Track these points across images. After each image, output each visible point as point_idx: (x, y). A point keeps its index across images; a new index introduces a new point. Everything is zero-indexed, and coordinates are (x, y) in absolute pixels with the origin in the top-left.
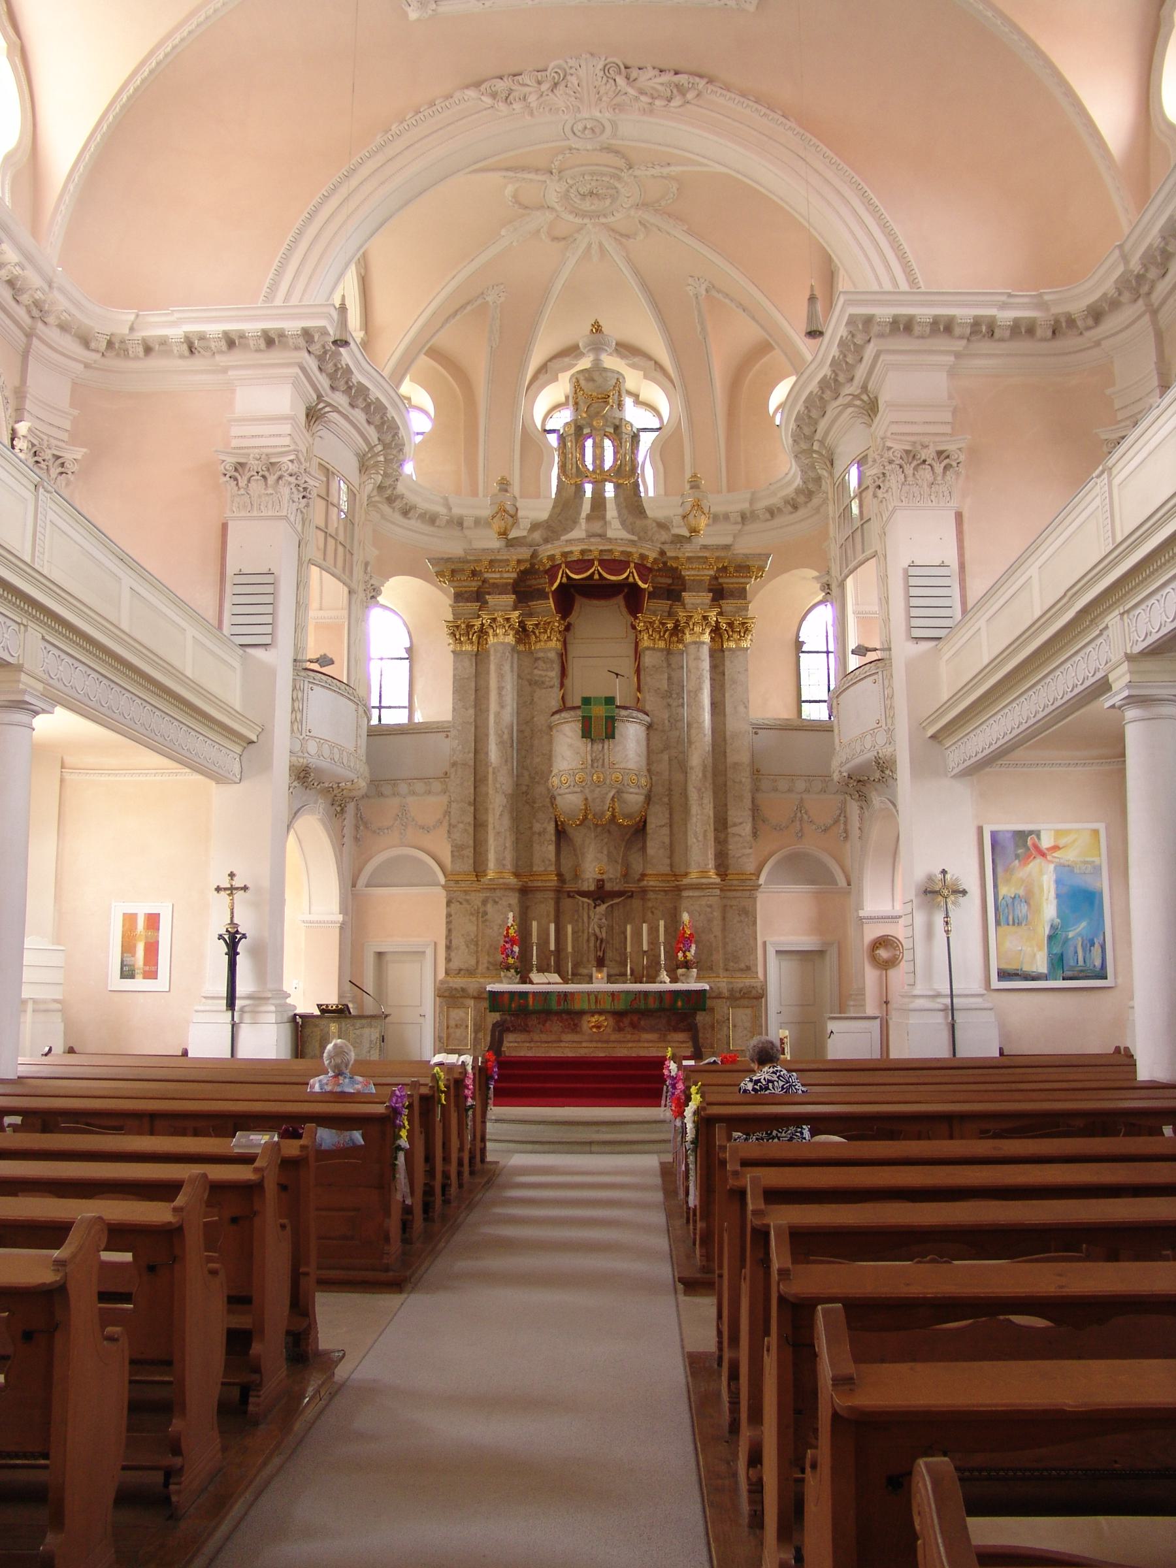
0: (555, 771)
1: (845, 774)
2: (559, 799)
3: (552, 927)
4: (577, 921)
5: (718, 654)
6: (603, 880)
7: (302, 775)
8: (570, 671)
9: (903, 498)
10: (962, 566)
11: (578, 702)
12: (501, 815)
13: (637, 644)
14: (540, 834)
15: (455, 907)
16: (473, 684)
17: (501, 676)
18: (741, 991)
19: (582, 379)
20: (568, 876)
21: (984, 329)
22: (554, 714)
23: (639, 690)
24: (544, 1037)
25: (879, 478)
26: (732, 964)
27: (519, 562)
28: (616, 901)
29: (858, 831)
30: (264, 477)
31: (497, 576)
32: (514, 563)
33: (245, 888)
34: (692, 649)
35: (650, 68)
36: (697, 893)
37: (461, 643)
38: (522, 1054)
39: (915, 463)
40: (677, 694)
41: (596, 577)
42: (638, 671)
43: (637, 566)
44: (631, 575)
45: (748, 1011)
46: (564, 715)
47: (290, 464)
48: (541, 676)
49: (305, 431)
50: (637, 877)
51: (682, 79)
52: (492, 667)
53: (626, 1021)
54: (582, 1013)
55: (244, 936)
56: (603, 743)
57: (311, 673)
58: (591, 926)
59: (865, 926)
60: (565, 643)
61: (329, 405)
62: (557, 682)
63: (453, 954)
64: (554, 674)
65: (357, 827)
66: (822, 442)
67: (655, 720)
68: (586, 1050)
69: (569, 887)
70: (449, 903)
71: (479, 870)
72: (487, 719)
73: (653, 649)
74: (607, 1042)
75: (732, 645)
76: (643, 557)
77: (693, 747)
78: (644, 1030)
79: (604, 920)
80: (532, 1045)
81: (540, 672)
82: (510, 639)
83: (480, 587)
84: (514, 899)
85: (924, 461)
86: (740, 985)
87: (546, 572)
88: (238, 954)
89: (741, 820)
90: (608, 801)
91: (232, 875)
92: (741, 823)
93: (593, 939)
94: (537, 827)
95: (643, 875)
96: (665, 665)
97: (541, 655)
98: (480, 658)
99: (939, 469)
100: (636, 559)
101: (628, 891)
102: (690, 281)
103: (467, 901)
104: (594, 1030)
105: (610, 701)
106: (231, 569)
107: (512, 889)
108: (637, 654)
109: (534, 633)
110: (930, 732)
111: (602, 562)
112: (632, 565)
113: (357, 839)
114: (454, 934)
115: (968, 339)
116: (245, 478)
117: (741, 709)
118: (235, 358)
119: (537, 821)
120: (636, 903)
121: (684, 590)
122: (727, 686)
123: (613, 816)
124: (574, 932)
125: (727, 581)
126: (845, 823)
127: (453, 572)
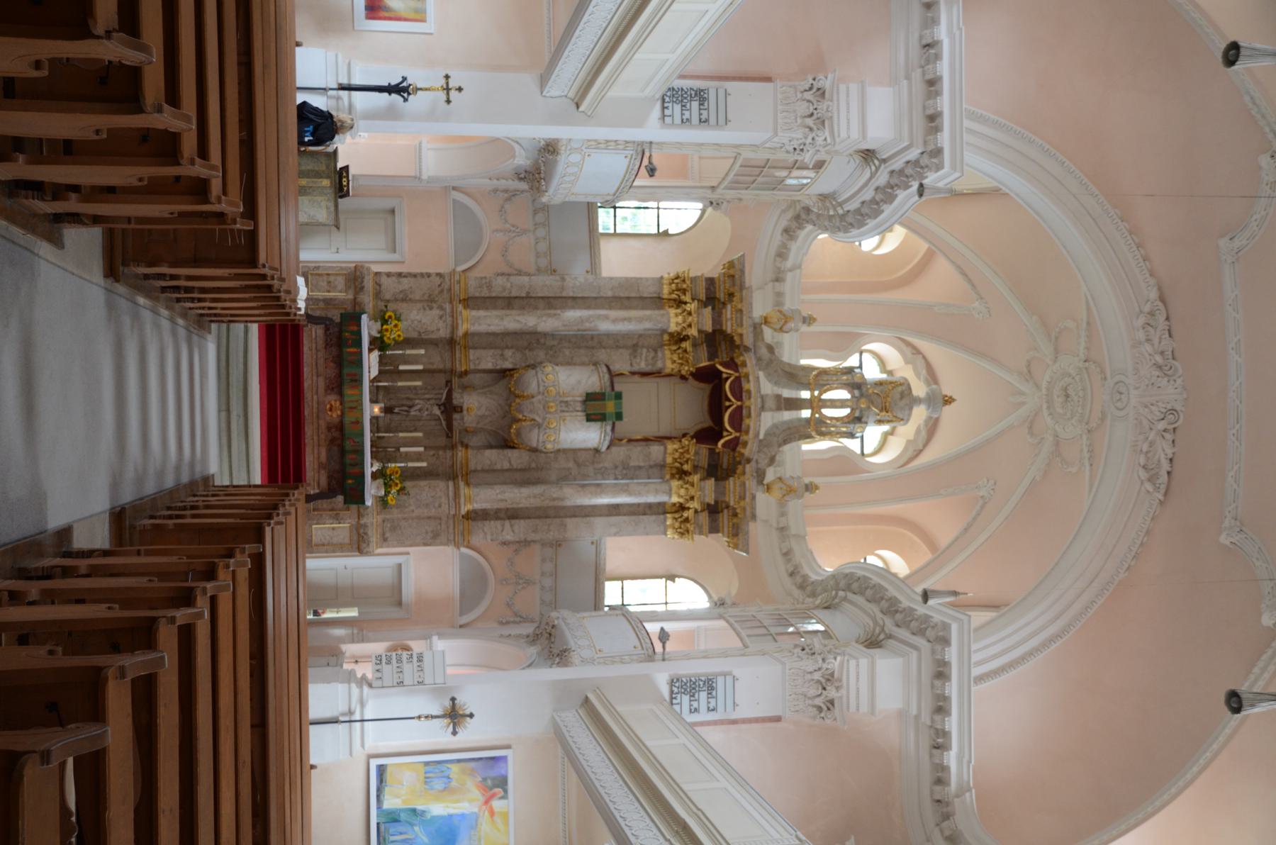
0: (557, 368)
1: (556, 622)
2: (533, 372)
3: (420, 367)
4: (426, 388)
5: (659, 510)
6: (461, 411)
7: (550, 148)
8: (645, 380)
9: (793, 670)
10: (734, 722)
11: (618, 388)
12: (518, 321)
13: (669, 438)
14: (502, 355)
15: (437, 280)
16: (633, 295)
17: (640, 320)
18: (366, 534)
19: (904, 388)
20: (465, 380)
21: (940, 740)
22: (607, 367)
23: (630, 441)
24: (321, 361)
25: (811, 649)
26: (389, 525)
27: (741, 335)
28: (444, 423)
29: (507, 634)
30: (812, 115)
31: (729, 316)
32: (739, 331)
33: (448, 101)
34: (665, 487)
35: (1173, 451)
36: (451, 494)
37: (670, 284)
38: (305, 342)
39: (823, 681)
40: (626, 474)
41: (727, 404)
42: (646, 440)
43: (737, 439)
44: (730, 434)
45: (347, 540)
46: (607, 376)
47: (823, 138)
48: (642, 354)
49: (855, 148)
50: (466, 441)
51: (1164, 478)
52: (648, 312)
53: (337, 434)
54: (341, 394)
55: (406, 100)
56: (582, 411)
57: (640, 157)
58: (421, 402)
59: (424, 641)
60: (670, 375)
61: (877, 169)
62: (636, 368)
63: (394, 278)
64: (643, 366)
65: (506, 191)
66: (845, 599)
67: (603, 455)
68: (309, 398)
69: (455, 381)
70: (439, 275)
71: (469, 302)
72: (603, 308)
73: (665, 453)
74: (318, 417)
75: (669, 522)
76: (745, 444)
77: (580, 489)
78: (329, 451)
79: (426, 413)
80: (314, 351)
81: (644, 355)
82: (673, 328)
83: (719, 300)
84: (444, 333)
85: (824, 689)
86: (370, 533)
87: (732, 359)
88: (390, 94)
89: (516, 531)
90: (532, 416)
91: (460, 89)
92: (513, 531)
93: (411, 403)
94: (508, 353)
95: (467, 446)
96: (652, 463)
97: (660, 354)
98: (657, 302)
99: (819, 701)
100: (744, 438)
101: (452, 433)
102: (992, 482)
103: (442, 291)
104: (328, 406)
105: (619, 416)
106: (730, 86)
107: (452, 332)
108: (661, 439)
109: (679, 349)
110: (592, 697)
111: (740, 408)
112: (738, 434)
113: (496, 191)
114: (412, 280)
115: (931, 727)
116: (810, 98)
117: (614, 530)
118: (919, 87)
119: (514, 353)
120: (442, 441)
121: (716, 480)
122: (633, 518)
123: (518, 421)
124: (415, 387)
125: (724, 517)
126: (514, 622)
127: (733, 276)
